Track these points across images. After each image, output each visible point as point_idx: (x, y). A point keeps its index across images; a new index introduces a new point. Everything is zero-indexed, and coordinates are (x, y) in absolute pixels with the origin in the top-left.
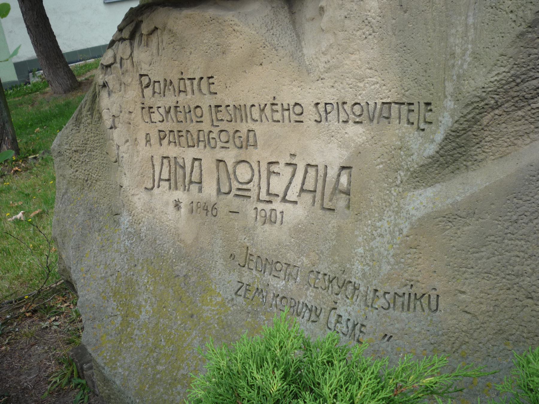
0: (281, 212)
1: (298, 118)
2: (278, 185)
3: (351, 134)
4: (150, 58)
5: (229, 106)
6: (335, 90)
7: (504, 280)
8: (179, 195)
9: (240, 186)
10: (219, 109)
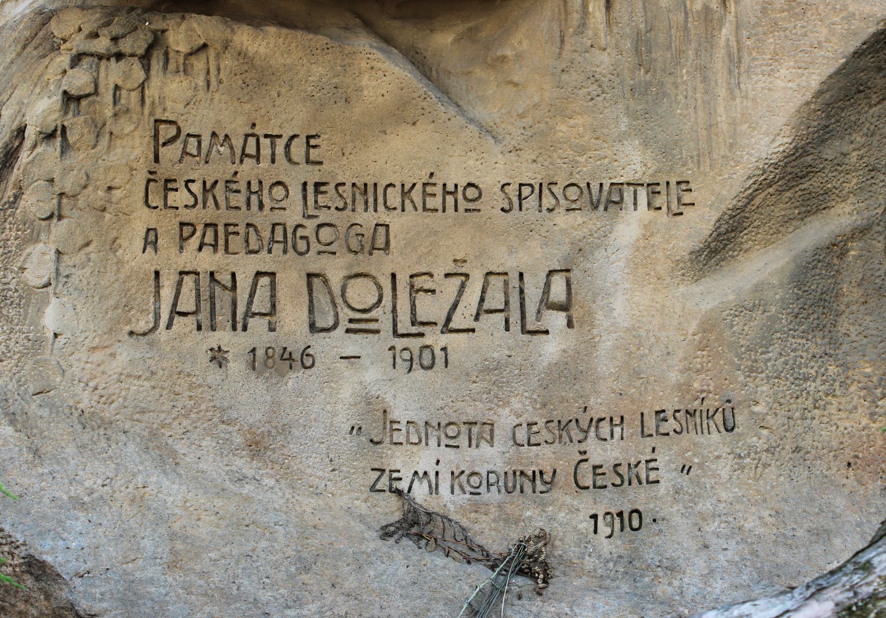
0: (442, 349)
1: (471, 206)
2: (431, 308)
3: (563, 225)
4: (190, 93)
5: (344, 184)
6: (539, 165)
7: (793, 386)
8: (223, 337)
9: (358, 316)
10: (323, 188)
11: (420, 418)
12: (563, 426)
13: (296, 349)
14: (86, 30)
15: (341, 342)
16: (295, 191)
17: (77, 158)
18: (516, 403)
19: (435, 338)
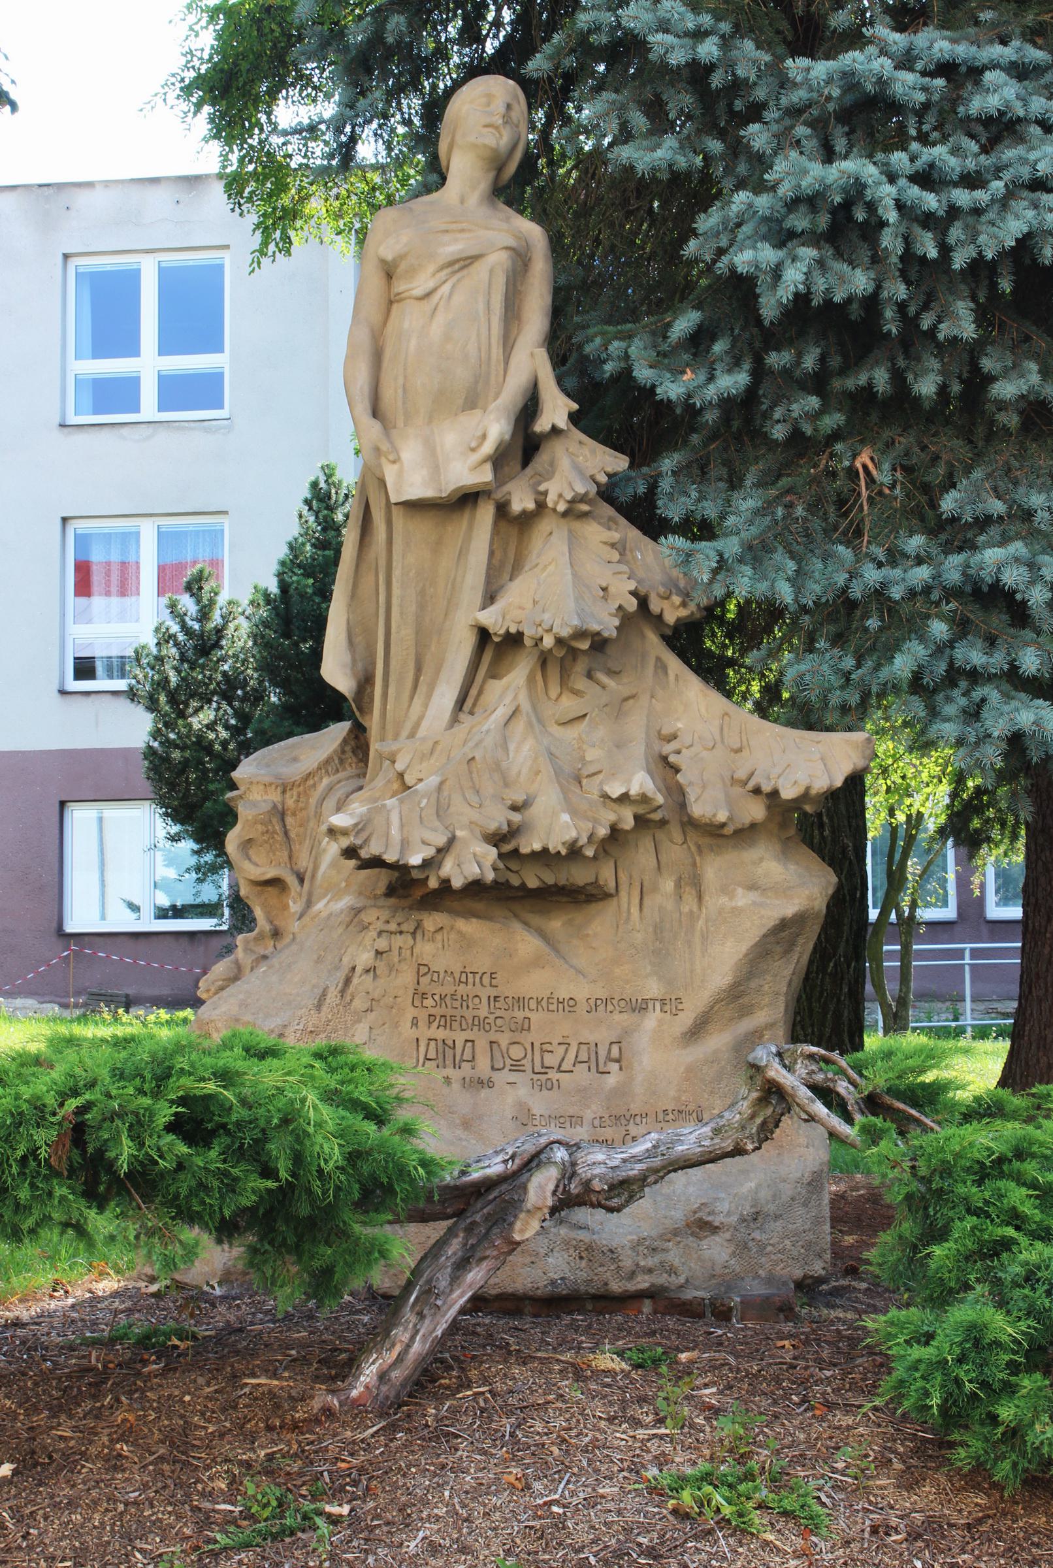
2: (550, 1060)
8: (449, 1071)
11: (546, 1114)
12: (617, 1118)
13: (485, 1078)
14: (383, 918)
15: (506, 1076)
16: (485, 1000)
17: (381, 982)
18: (594, 1107)
19: (553, 1075)
